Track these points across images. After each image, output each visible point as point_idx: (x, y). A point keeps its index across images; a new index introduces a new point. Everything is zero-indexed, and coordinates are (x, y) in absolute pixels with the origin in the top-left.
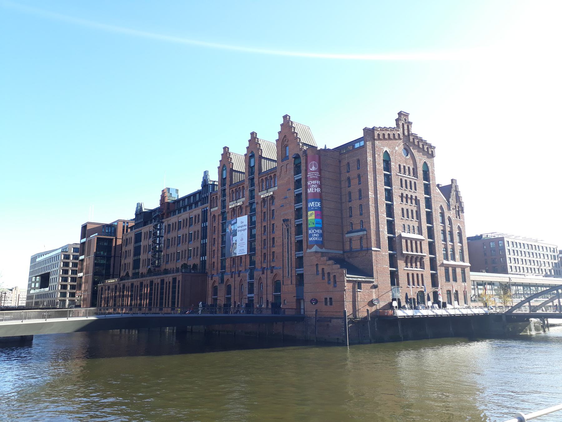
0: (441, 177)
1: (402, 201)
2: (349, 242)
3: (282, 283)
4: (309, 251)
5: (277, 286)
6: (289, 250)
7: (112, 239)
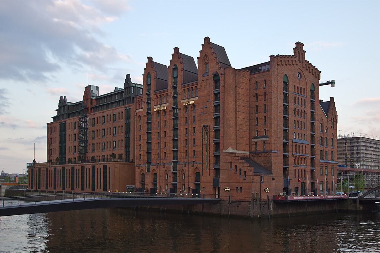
1: (295, 114)
4: (224, 151)
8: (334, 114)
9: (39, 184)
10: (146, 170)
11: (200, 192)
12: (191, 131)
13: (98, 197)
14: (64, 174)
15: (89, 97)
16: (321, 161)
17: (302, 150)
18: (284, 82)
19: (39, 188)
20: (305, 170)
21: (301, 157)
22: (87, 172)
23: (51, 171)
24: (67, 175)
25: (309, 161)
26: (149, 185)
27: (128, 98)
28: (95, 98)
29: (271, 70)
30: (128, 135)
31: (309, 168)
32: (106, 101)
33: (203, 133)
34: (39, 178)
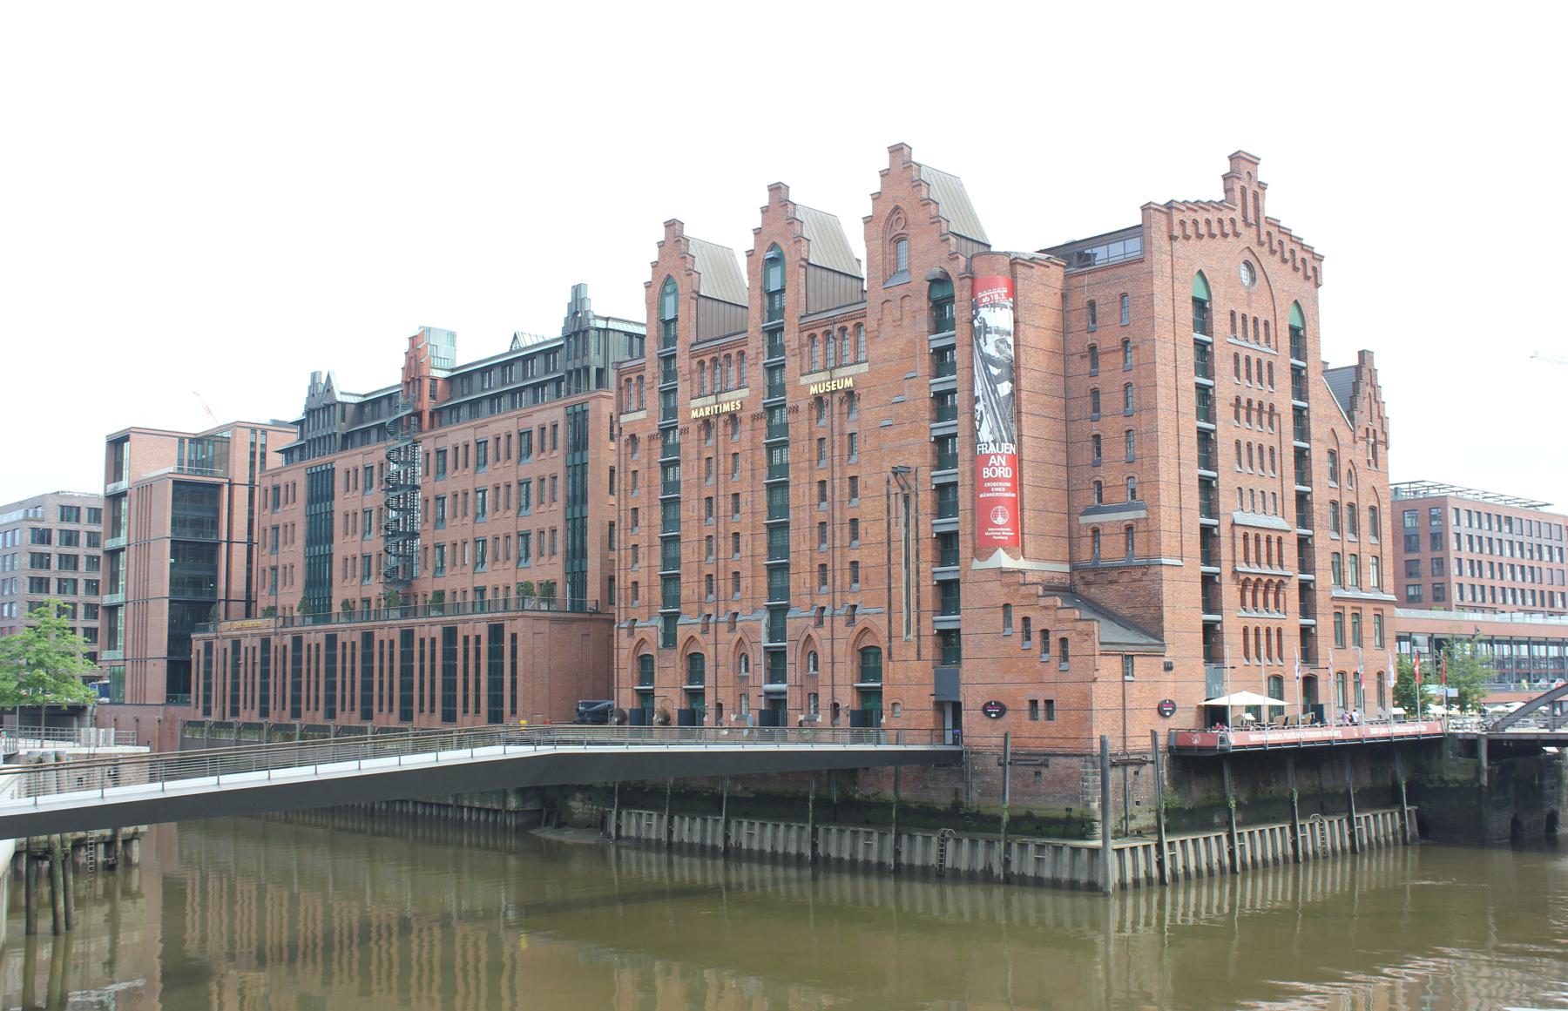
0: (1335, 348)
1: (1237, 417)
2: (1089, 540)
3: (885, 653)
4: (977, 565)
5: (869, 661)
6: (912, 558)
7: (219, 486)
8: (1375, 412)
9: (235, 699)
10: (660, 642)
11: (884, 720)
12: (840, 489)
13: (118, 742)
14: (331, 659)
15: (424, 373)
16: (1334, 594)
17: (1269, 555)
18: (1195, 300)
19: (235, 712)
20: (1279, 631)
21: (1265, 579)
22: (382, 654)
23: (280, 649)
24: (381, 660)
25: (1292, 595)
26: (670, 693)
27: (578, 371)
28: (445, 374)
29: (1147, 257)
30: (577, 509)
31: (1292, 622)
32: (494, 385)
33: (893, 497)
34: (236, 674)
